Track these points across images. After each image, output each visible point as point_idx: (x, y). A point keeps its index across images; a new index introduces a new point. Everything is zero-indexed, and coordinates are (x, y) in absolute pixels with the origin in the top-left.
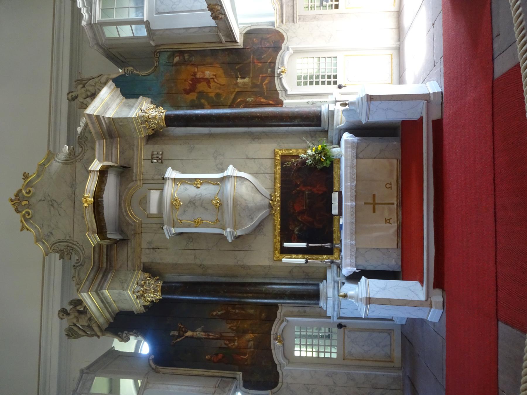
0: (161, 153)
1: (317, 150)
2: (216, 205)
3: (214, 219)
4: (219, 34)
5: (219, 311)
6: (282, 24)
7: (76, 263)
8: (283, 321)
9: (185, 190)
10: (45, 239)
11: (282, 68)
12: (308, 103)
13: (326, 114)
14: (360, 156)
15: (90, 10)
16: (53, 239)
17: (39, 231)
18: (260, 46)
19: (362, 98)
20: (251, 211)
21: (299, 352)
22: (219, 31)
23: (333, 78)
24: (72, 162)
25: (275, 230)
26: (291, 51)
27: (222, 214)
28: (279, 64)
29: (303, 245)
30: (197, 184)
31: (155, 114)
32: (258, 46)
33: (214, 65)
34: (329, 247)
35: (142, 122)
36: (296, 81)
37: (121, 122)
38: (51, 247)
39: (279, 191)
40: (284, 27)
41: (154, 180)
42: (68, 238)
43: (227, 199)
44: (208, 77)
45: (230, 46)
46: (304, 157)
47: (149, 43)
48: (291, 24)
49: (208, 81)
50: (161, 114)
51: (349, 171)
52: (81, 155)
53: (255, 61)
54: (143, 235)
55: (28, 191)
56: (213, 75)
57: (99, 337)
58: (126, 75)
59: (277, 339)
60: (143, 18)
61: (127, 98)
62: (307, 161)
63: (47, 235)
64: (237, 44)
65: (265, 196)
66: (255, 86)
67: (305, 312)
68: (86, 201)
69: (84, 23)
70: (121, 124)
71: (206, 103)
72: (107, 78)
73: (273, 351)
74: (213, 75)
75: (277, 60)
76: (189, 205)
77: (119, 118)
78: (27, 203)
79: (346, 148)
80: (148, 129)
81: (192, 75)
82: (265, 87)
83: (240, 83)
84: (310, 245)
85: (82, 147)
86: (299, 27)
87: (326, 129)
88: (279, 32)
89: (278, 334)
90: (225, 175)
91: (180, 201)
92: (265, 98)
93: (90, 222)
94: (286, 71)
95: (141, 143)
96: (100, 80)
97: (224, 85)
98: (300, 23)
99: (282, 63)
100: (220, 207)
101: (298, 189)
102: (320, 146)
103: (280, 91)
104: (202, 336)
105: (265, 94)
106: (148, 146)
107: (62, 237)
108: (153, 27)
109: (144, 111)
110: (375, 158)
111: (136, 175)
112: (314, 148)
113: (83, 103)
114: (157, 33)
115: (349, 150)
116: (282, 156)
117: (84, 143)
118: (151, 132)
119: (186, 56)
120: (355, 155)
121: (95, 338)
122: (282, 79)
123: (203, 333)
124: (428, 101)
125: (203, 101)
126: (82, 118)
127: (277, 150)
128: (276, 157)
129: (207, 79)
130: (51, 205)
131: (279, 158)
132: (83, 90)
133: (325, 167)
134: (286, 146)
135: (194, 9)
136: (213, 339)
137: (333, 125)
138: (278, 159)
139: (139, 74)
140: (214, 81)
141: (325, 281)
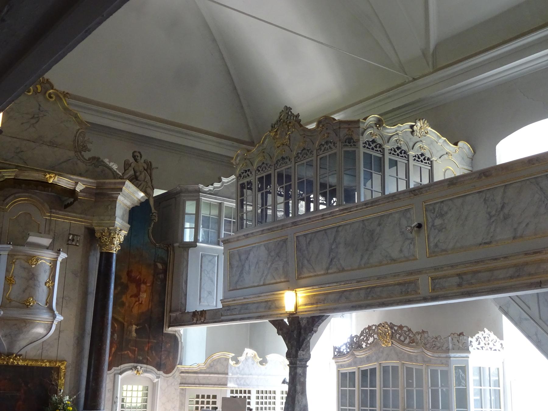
0: (78, 244)
1: (67, 405)
2: (27, 300)
3: (12, 297)
4: (179, 312)
6: (180, 372)
9: (45, 271)
11: (141, 371)
15: (210, 193)
22: (181, 312)
23: (212, 401)
24: (75, 147)
27: (17, 307)
28: (145, 367)
30: (49, 283)
31: (115, 243)
32: (163, 347)
33: (150, 303)
35: (110, 230)
37: (112, 208)
39: (23, 364)
40: (177, 374)
44: (141, 296)
47: (177, 242)
48: (179, 381)
49: (137, 295)
50: (115, 249)
52: (82, 158)
53: (150, 344)
55: (52, 96)
56: (142, 301)
58: (151, 214)
60: (199, 243)
61: (130, 211)
62: (56, 395)
64: (167, 327)
65: (22, 349)
68: (51, 177)
69: (201, 186)
70: (109, 207)
72: (150, 195)
74: (142, 301)
75: (149, 366)
76: (31, 274)
77: (116, 208)
80: (102, 234)
81: (144, 280)
82: (126, 352)
83: (132, 328)
86: (175, 389)
88: (173, 369)
93: (28, 175)
94: (138, 374)
95: (87, 222)
96: (149, 187)
97: (131, 310)
98: (179, 390)
99: (146, 371)
100: (25, 305)
101: (23, 385)
103: (120, 369)
105: (119, 353)
106: (83, 230)
108: (191, 250)
109: (120, 233)
113: (129, 166)
114: (185, 253)
117: (93, 164)
118: (98, 235)
119: (161, 276)
122: (132, 370)
126: (117, 165)
128: (58, 362)
129: (139, 294)
134: (68, 374)
135: (202, 290)
138: (56, 365)
139: (150, 227)
140: (136, 301)
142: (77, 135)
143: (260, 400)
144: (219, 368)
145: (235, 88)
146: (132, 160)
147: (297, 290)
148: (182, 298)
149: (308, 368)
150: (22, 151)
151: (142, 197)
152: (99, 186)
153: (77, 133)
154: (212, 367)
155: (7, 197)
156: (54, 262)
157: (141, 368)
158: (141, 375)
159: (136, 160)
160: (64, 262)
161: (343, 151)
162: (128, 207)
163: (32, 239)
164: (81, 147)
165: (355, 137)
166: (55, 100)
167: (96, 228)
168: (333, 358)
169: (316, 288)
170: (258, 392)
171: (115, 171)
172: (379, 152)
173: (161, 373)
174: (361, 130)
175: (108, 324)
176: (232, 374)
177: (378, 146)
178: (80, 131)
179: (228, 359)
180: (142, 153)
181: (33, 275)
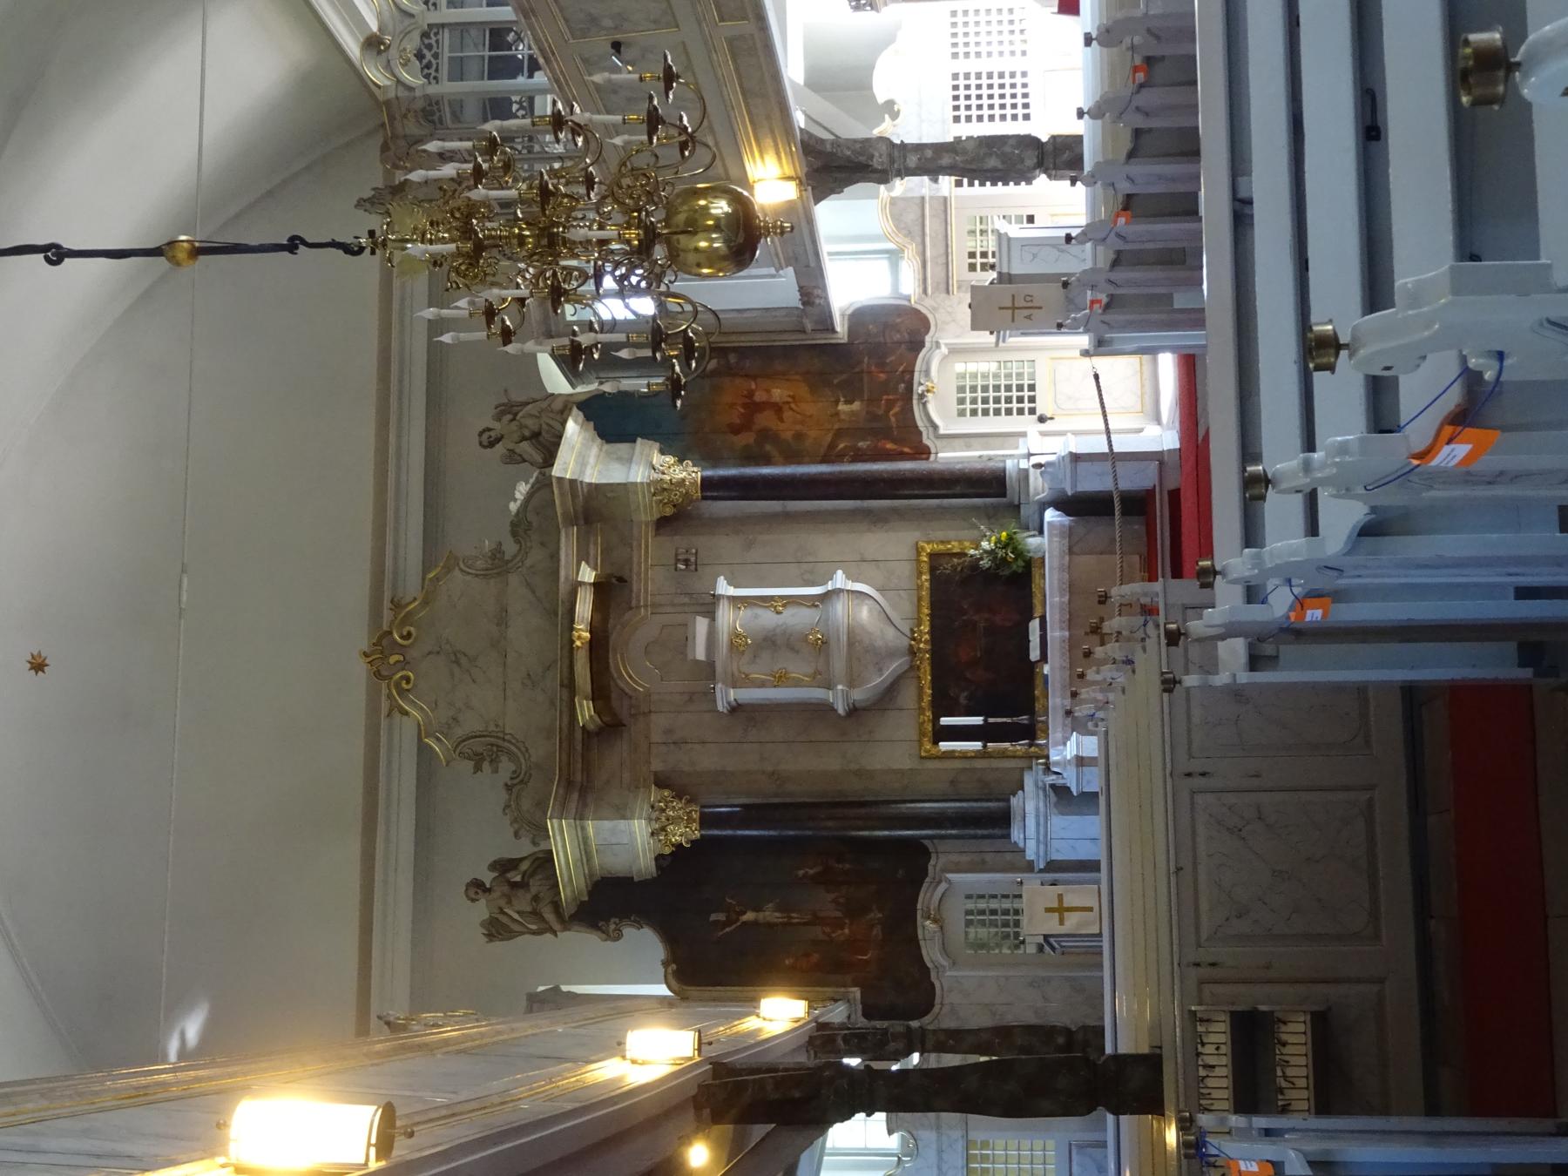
0: (694, 551)
1: (998, 541)
3: (810, 670)
5: (811, 868)
7: (512, 778)
8: (940, 882)
10: (442, 733)
12: (980, 457)
13: (1014, 475)
14: (1075, 549)
16: (459, 732)
17: (428, 716)
18: (882, 339)
19: (1063, 457)
20: (880, 656)
21: (1010, 311)
24: (498, 574)
25: (920, 699)
26: (944, 350)
29: (977, 720)
34: (1026, 722)
36: (954, 407)
38: (457, 746)
39: (928, 623)
40: (928, 302)
41: (673, 605)
42: (492, 728)
43: (838, 630)
45: (821, 340)
46: (975, 555)
48: (944, 295)
49: (778, 409)
50: (694, 475)
51: (1056, 577)
52: (518, 558)
54: (653, 717)
55: (405, 633)
56: (789, 396)
57: (555, 933)
59: (929, 918)
61: (609, 441)
63: (447, 723)
64: (834, 336)
66: (873, 417)
67: (983, 862)
68: (579, 638)
71: (775, 453)
73: (922, 943)
74: (789, 396)
75: (917, 368)
78: (402, 659)
79: (1050, 535)
82: (893, 419)
84: (991, 720)
85: (520, 542)
86: (959, 303)
87: (1016, 503)
89: (932, 908)
90: (830, 588)
91: (746, 637)
92: (894, 441)
98: (962, 295)
99: (927, 373)
102: (1004, 534)
104: (776, 920)
106: (659, 538)
107: (478, 727)
110: (1101, 554)
111: (638, 596)
112: (993, 538)
115: (1056, 539)
116: (932, 556)
118: (669, 511)
119: (732, 358)
120: (1066, 549)
121: (548, 936)
123: (777, 914)
124: (1161, 464)
125: (768, 447)
127: (921, 544)
130: (454, 662)
131: (926, 559)
132: (514, 426)
133: (1015, 573)
134: (940, 535)
136: (799, 924)
137: (1028, 495)
141: (1020, 792)
142: (474, 572)
143: (972, 49)
144: (911, 216)
145: (270, 193)
146: (500, 448)
147: (751, 180)
148: (776, 316)
149: (906, 141)
150: (529, 675)
151: (576, 422)
152: (571, 521)
153: (469, 573)
154: (910, 233)
155: (623, 690)
156: (734, 600)
157: (920, 384)
158: (935, 381)
159: (498, 440)
160: (733, 582)
161: (454, 126)
162: (601, 450)
163: (700, 654)
164: (497, 561)
165: (420, 104)
166: (411, 626)
167: (656, 516)
168: (878, 11)
169: (741, 135)
170: (957, 119)
171: (532, 487)
172: (440, 37)
173: (928, 339)
174: (402, 93)
175: (841, 472)
176: (922, 187)
177: (426, 41)
178: (462, 566)
179: (892, 198)
180: (481, 429)
181: (765, 639)
